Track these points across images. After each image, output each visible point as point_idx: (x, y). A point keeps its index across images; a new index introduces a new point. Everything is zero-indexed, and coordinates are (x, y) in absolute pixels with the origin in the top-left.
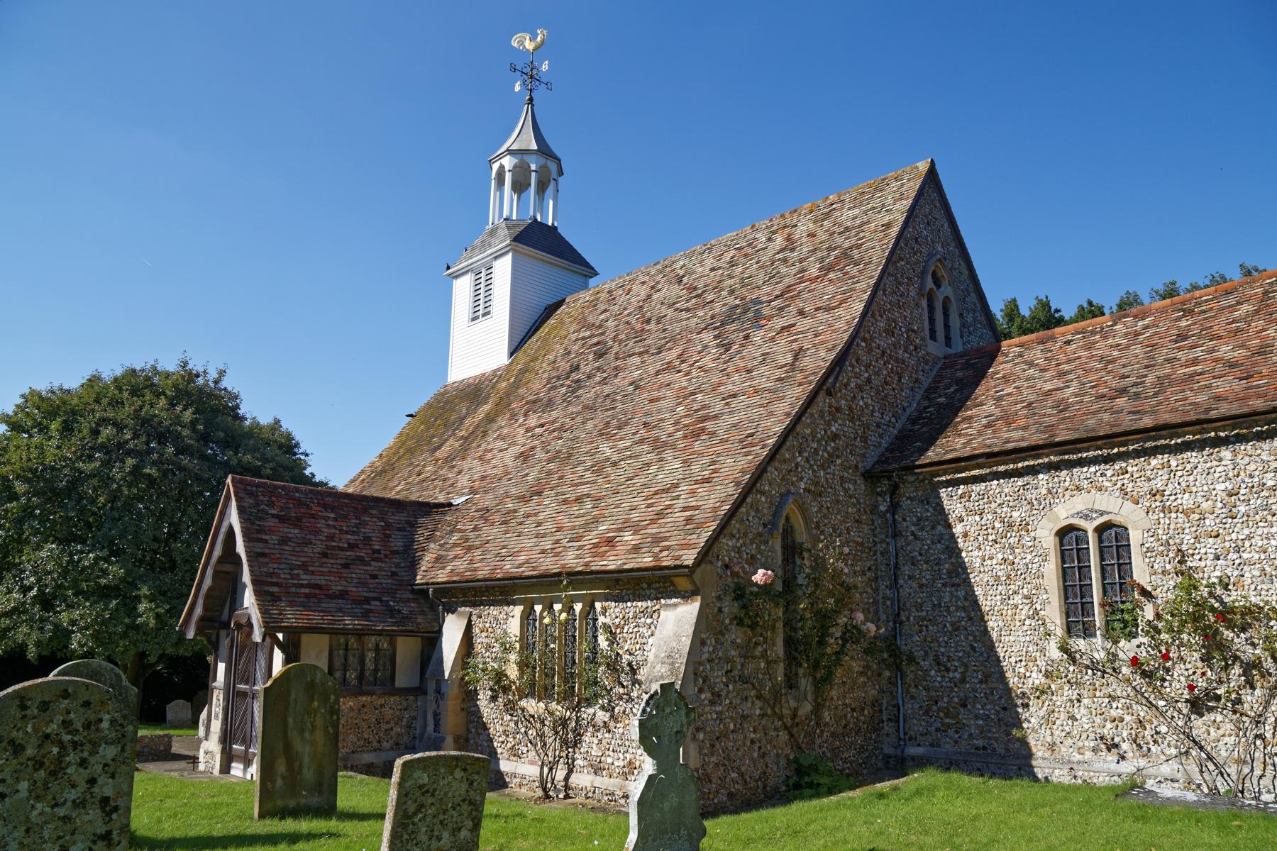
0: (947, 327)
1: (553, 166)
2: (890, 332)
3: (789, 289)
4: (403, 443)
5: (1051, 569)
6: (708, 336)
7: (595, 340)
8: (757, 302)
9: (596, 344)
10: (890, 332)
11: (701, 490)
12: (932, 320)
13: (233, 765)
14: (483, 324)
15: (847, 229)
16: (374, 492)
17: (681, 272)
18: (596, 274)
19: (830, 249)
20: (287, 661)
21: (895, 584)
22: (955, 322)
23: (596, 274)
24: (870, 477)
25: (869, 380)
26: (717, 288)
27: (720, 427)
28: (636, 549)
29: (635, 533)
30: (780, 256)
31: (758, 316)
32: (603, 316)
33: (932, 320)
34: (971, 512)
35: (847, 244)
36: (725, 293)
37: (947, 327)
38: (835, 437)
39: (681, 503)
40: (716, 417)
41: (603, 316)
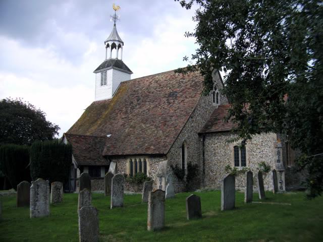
0: (217, 99)
1: (121, 44)
2: (205, 103)
3: (183, 90)
4: (85, 118)
5: (232, 154)
6: (165, 99)
7: (136, 95)
8: (176, 92)
9: (136, 97)
10: (205, 103)
11: (167, 138)
12: (214, 98)
13: (273, 135)
14: (104, 87)
15: (196, 76)
16: (81, 132)
17: (157, 80)
18: (132, 73)
19: (192, 81)
20: (81, 172)
21: (204, 156)
22: (219, 98)
23: (132, 73)
24: (200, 134)
25: (200, 114)
26: (167, 86)
27: (170, 123)
28: (155, 150)
29: (154, 146)
30: (181, 80)
31: (176, 96)
32: (137, 89)
33: (214, 98)
34: (218, 142)
35: (196, 81)
36: (168, 88)
37: (217, 99)
38: (192, 126)
39: (163, 141)
40: (168, 121)
41: (137, 89)
